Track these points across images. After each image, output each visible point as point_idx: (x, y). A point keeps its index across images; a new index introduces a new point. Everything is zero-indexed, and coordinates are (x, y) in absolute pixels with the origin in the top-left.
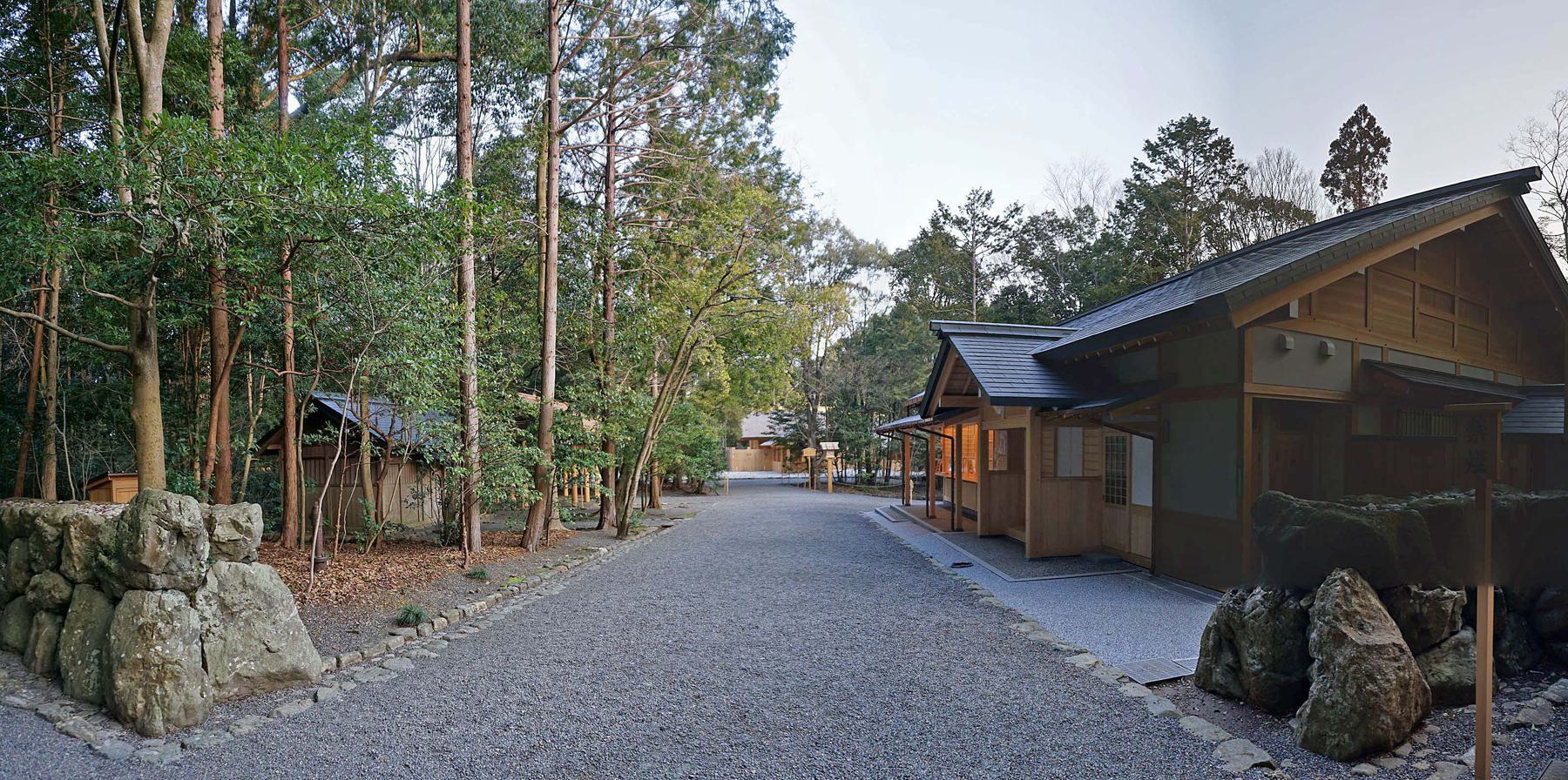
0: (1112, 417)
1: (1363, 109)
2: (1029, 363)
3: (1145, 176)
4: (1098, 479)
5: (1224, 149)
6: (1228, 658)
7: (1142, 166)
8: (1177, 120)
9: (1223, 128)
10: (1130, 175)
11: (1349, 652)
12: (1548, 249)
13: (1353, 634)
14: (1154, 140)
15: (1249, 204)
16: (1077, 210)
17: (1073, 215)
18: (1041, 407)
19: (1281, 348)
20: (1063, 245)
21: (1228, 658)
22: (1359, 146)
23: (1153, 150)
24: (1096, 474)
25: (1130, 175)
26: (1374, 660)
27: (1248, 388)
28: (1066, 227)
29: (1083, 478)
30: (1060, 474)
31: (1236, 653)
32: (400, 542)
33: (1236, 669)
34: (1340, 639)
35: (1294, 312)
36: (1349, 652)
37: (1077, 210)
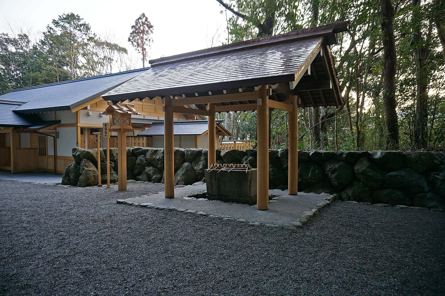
0: (41, 131)
1: (144, 15)
2: (11, 113)
3: (52, 31)
4: (37, 148)
5: (87, 28)
6: (68, 178)
7: (51, 28)
8: (66, 13)
9: (86, 19)
10: (46, 30)
11: (85, 171)
12: (340, 23)
13: (86, 168)
14: (57, 19)
15: (99, 44)
16: (19, 35)
17: (17, 37)
18: (15, 127)
19: (88, 115)
20: (12, 49)
21: (68, 178)
22: (141, 29)
23: (56, 23)
24: (35, 147)
25: (46, 30)
26: (89, 172)
27: (78, 125)
28: (14, 42)
29: (31, 148)
30: (22, 147)
31: (69, 176)
32: (154, 124)
33: (69, 180)
34: (84, 169)
35: (89, 108)
36: (85, 171)
37: (19, 35)
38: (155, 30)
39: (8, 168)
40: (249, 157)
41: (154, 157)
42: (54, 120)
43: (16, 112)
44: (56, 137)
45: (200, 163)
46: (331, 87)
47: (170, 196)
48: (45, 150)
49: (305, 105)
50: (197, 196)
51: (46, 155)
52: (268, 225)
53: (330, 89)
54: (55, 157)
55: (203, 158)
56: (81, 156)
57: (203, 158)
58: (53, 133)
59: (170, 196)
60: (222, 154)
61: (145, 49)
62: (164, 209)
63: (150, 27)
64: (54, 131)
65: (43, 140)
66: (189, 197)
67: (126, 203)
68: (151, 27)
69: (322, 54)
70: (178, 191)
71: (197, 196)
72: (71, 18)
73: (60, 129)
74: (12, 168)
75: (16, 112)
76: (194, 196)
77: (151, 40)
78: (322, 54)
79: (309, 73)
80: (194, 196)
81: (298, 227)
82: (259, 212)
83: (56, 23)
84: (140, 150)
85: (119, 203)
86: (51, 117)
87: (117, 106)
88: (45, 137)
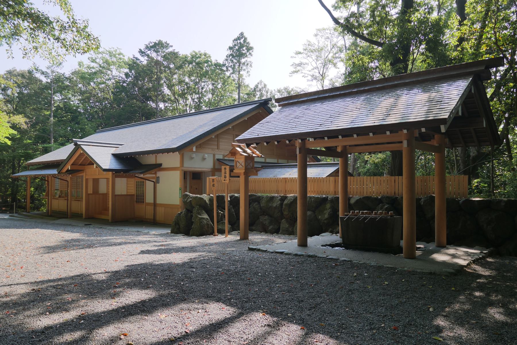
4: (134, 195)
6: (178, 227)
21: (178, 227)
23: (141, 52)
29: (127, 195)
38: (254, 52)
39: (103, 217)
40: (385, 205)
41: (270, 205)
42: (154, 163)
43: (115, 156)
44: (157, 181)
45: (325, 212)
46: (485, 126)
47: (303, 244)
48: (143, 196)
49: (453, 145)
50: (333, 246)
51: (143, 202)
52: (419, 271)
53: (484, 128)
54: (155, 204)
55: (328, 206)
56: (193, 203)
57: (328, 206)
58: (153, 178)
59: (303, 244)
60: (352, 201)
61: (242, 76)
62: (302, 255)
63: (249, 49)
64: (154, 175)
65: (141, 186)
66: (322, 246)
67: (259, 250)
68: (252, 48)
69: (473, 91)
70: (312, 241)
71: (333, 246)
72: (158, 46)
73: (160, 174)
74: (109, 217)
75: (115, 156)
76: (330, 245)
77: (249, 65)
78: (473, 91)
79: (460, 114)
80: (330, 245)
81: (451, 273)
82: (406, 260)
83: (141, 52)
84: (254, 197)
85: (250, 249)
86: (151, 160)
87: (250, 149)
88: (143, 182)
